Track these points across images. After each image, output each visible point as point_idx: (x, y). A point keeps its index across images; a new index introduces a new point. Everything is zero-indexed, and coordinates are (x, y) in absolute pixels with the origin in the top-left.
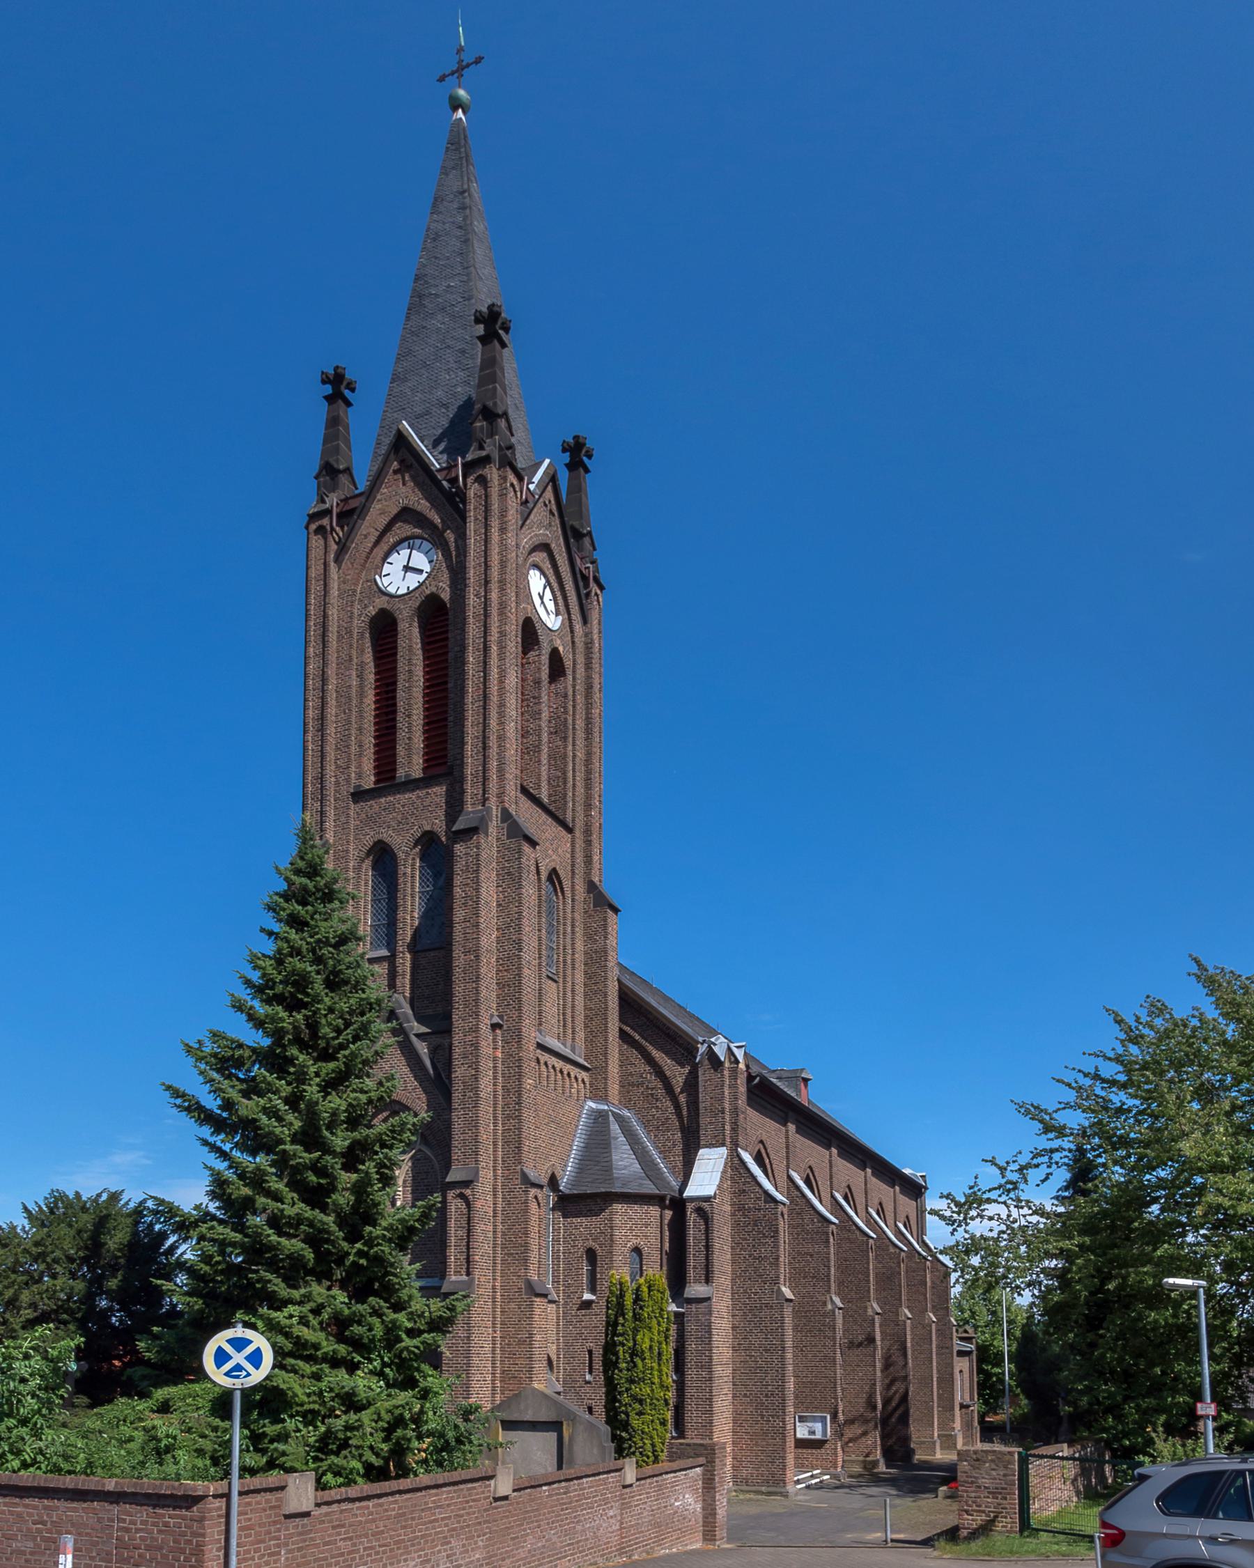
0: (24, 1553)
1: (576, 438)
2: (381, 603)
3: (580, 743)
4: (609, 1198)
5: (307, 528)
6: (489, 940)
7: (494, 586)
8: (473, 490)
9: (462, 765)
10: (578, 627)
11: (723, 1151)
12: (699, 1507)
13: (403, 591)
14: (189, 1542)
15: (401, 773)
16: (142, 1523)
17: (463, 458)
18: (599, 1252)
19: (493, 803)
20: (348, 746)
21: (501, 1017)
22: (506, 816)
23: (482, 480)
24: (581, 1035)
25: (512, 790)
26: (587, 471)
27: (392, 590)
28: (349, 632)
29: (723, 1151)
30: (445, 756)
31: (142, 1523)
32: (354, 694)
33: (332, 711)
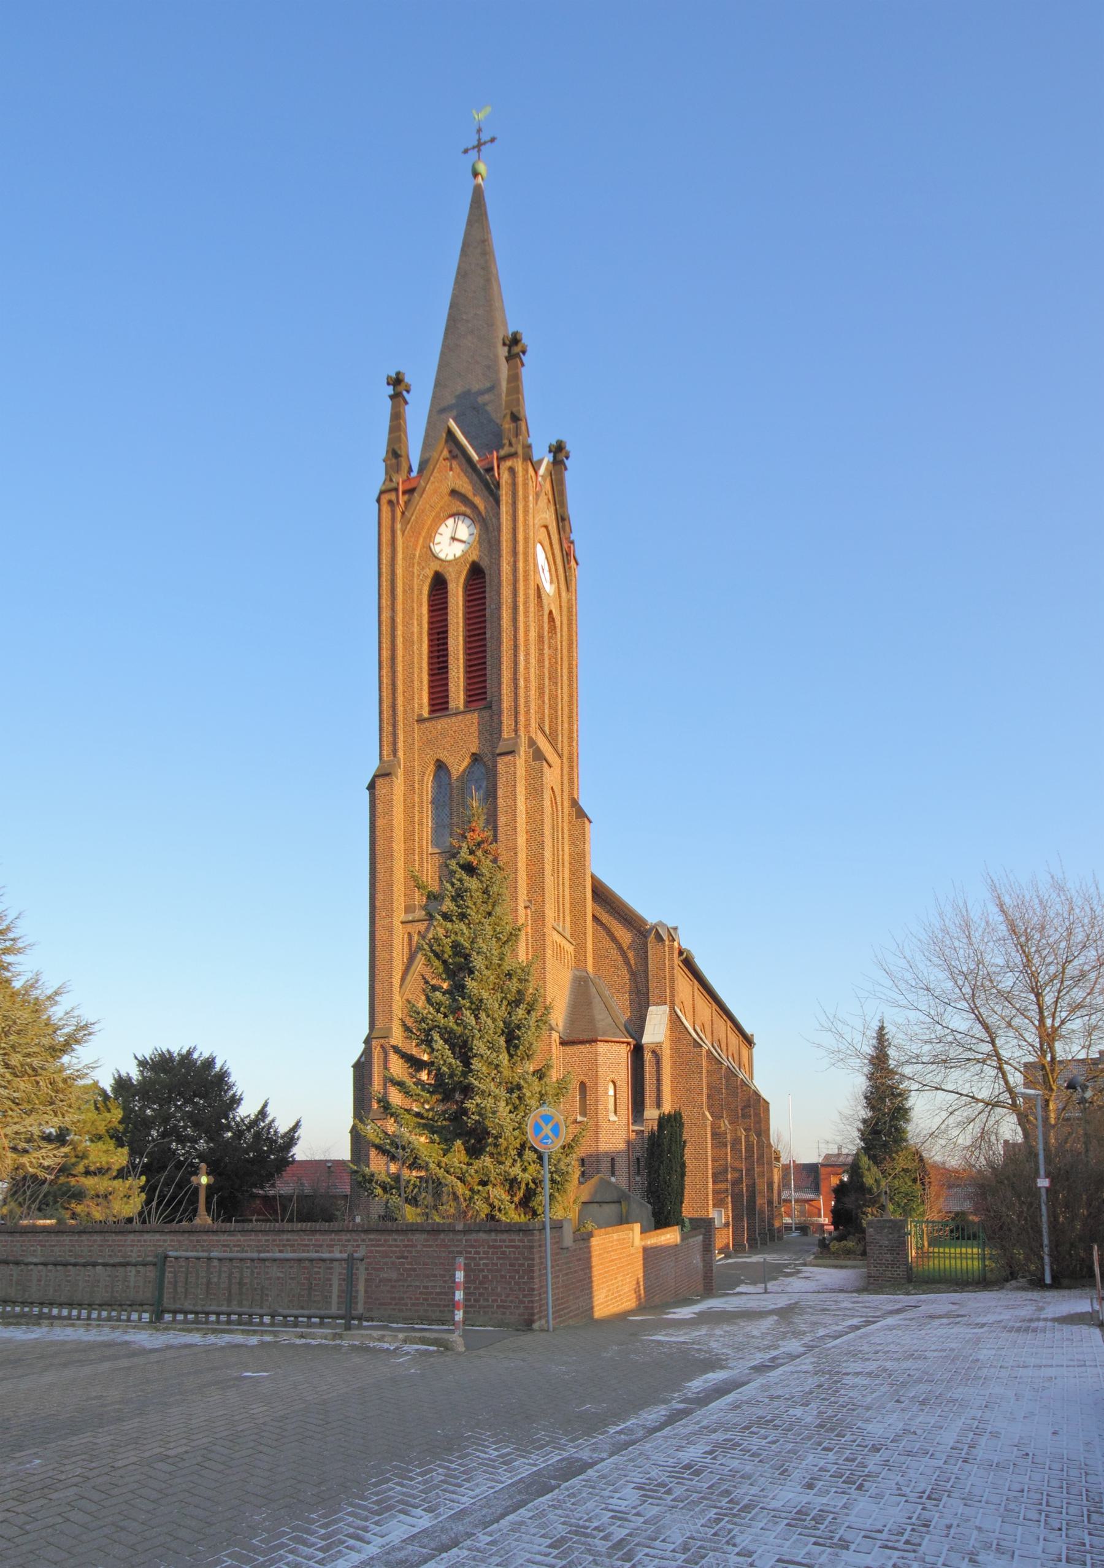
0: (390, 1280)
1: (398, 374)
2: (435, 566)
3: (565, 687)
4: (596, 1041)
5: (378, 501)
6: (521, 840)
7: (521, 557)
8: (505, 477)
9: (500, 701)
10: (564, 593)
11: (666, 1008)
12: (701, 1265)
13: (450, 557)
14: (523, 1265)
15: (452, 705)
16: (484, 1253)
17: (498, 452)
18: (588, 1084)
19: (522, 733)
20: (412, 682)
21: (530, 901)
22: (532, 743)
23: (512, 470)
24: (568, 918)
25: (534, 725)
26: (406, 403)
27: (442, 556)
28: (412, 589)
29: (666, 1008)
30: (485, 693)
31: (484, 1253)
32: (415, 639)
33: (400, 652)
